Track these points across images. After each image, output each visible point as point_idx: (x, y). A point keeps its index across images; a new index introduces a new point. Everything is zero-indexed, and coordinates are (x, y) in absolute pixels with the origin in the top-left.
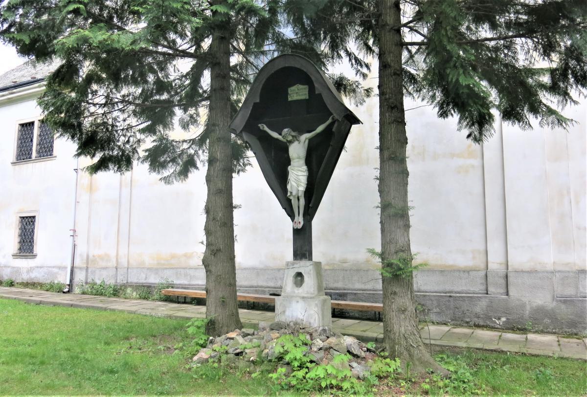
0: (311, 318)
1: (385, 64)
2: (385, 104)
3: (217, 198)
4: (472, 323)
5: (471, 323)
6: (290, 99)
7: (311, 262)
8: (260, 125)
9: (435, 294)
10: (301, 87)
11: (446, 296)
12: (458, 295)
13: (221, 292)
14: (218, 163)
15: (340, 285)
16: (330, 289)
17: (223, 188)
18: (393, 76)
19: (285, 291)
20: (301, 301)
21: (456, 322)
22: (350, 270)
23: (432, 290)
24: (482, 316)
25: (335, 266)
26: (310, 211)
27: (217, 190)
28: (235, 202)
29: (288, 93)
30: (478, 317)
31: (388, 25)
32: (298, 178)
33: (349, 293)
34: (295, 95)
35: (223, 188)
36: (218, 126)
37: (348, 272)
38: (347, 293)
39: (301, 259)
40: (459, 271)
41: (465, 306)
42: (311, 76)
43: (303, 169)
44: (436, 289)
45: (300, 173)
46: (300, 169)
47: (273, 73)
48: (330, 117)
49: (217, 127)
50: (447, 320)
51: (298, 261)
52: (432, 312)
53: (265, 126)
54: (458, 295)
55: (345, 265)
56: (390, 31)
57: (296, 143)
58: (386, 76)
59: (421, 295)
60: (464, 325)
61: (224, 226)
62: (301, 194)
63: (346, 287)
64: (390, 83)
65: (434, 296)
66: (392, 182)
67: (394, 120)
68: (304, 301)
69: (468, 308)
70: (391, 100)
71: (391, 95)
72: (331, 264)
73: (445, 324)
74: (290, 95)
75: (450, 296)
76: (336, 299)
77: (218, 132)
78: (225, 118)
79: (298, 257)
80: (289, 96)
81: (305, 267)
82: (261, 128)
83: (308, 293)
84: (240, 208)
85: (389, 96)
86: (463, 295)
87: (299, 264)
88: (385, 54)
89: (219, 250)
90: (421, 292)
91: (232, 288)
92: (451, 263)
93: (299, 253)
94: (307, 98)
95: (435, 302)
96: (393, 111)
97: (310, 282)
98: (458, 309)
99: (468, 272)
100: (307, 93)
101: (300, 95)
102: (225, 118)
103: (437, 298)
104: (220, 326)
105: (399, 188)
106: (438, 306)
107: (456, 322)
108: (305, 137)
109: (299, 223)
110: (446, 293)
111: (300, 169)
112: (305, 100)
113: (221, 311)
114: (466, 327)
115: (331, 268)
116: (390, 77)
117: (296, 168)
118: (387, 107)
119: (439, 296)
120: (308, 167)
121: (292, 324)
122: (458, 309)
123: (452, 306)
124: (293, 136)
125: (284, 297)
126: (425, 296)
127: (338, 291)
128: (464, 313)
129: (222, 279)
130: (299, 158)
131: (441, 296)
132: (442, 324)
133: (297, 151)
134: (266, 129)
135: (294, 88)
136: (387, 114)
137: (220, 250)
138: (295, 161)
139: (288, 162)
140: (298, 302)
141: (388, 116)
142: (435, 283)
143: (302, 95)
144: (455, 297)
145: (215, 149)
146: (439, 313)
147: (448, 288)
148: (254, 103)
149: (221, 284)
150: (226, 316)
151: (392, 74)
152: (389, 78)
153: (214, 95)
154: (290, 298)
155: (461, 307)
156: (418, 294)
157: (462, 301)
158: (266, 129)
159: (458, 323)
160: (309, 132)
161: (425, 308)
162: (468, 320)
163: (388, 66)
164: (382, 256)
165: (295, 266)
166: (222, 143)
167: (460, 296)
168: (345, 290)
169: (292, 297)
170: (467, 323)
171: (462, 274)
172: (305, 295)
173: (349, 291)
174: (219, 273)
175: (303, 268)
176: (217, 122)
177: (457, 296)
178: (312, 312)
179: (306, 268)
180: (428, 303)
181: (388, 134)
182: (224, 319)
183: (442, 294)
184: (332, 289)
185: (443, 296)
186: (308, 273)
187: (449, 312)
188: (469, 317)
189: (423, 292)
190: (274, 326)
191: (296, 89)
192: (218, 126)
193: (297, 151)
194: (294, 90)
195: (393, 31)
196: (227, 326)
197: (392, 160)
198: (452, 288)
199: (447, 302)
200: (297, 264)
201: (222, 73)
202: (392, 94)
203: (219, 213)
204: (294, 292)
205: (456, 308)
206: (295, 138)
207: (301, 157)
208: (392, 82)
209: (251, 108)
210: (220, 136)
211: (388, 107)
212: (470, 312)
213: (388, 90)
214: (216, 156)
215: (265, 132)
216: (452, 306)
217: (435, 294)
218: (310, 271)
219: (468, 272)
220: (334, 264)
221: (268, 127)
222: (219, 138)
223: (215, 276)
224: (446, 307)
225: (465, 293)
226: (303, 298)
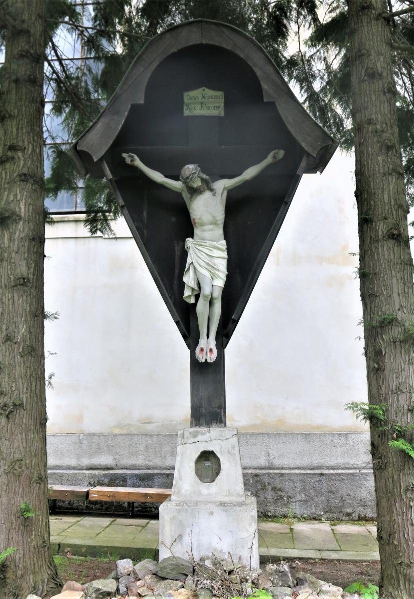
0: (243, 547)
1: (371, 71)
2: (375, 139)
3: (16, 295)
4: (355, 516)
5: (353, 515)
6: (186, 113)
7: (226, 433)
8: (124, 155)
9: (296, 471)
10: (209, 92)
11: (314, 474)
12: (332, 471)
13: (22, 497)
14: (21, 222)
15: (140, 461)
16: (122, 469)
17: (31, 276)
18: (387, 94)
19: (179, 492)
20: (217, 510)
21: (331, 515)
22: (157, 435)
23: (292, 465)
24: (369, 503)
25: (132, 429)
26: (225, 333)
27: (19, 279)
28: (48, 308)
29: (183, 102)
30: (365, 506)
31: (374, 9)
32: (207, 261)
33: (157, 474)
34: (199, 107)
35: (31, 276)
36: (23, 150)
37: (155, 438)
38: (153, 475)
39: (209, 423)
40: (333, 434)
41: (344, 489)
42: (254, 68)
43: (222, 245)
44: (298, 462)
45: (216, 253)
46: (215, 244)
47: (175, 52)
48: (274, 150)
49: (20, 154)
50: (319, 512)
51: (204, 429)
52: (294, 500)
53: (136, 157)
54: (332, 471)
55: (150, 427)
56: (377, 19)
57: (207, 195)
58: (374, 92)
59: (276, 474)
60: (344, 518)
61: (30, 354)
62: (218, 294)
63: (150, 464)
64: (382, 106)
65: (297, 474)
66: (394, 280)
67: (394, 170)
68: (226, 511)
69: (348, 492)
70: (385, 135)
71: (384, 126)
72: (126, 426)
73: (315, 519)
74: (188, 105)
75: (322, 474)
76: (134, 486)
77: (22, 163)
78: (35, 138)
79: (203, 421)
80: (185, 108)
81: (210, 438)
82: (128, 161)
83: (230, 494)
84: (56, 318)
85: (382, 127)
86: (340, 471)
87: (208, 434)
88: (369, 55)
89: (18, 406)
90: (274, 469)
91: (42, 486)
92: (319, 421)
93: (204, 411)
94: (222, 114)
95: (298, 485)
96: (390, 153)
97: (231, 475)
98: (334, 493)
99: (346, 435)
100: (222, 105)
101: (207, 108)
102: (35, 138)
103: (301, 477)
104: (19, 573)
105: (406, 290)
106: (304, 490)
107: (331, 515)
108: (222, 185)
109: (211, 350)
110: (312, 469)
111: (215, 244)
112: (219, 117)
113: (20, 538)
114: (347, 522)
115: (124, 432)
116: (382, 96)
117: (208, 243)
118: (379, 145)
119: (304, 474)
120: (228, 243)
121: (208, 563)
122: (334, 493)
123: (324, 490)
124: (203, 180)
125: (178, 505)
126: (282, 475)
127: (136, 472)
128: (344, 499)
129: (24, 468)
130: (215, 223)
131: (307, 474)
132: (311, 519)
133: (208, 209)
134: (138, 163)
135: (197, 93)
136: (380, 158)
137: (21, 405)
138: (206, 227)
139: (187, 228)
140: (212, 513)
141: (381, 162)
142: (296, 453)
143: (213, 108)
144: (329, 475)
145: (16, 195)
146: (304, 502)
147: (316, 461)
148: (133, 106)
149: (22, 478)
150: (32, 549)
151: (386, 90)
152: (379, 96)
153: (14, 92)
154: (191, 506)
155: (338, 491)
156: (271, 471)
157: (339, 480)
158: (138, 163)
159: (335, 515)
160: (230, 177)
161: (282, 494)
162: (349, 510)
163: (377, 75)
164: (372, 418)
165: (200, 438)
166: (29, 186)
167: (336, 474)
168: (149, 469)
169: (196, 503)
170: (349, 515)
171: (337, 439)
172: (226, 499)
173: (156, 471)
174: (17, 456)
175: (217, 442)
176: (20, 143)
177: (332, 474)
178: (244, 535)
179: (223, 443)
180: (288, 486)
181: (383, 192)
182: (27, 556)
183: (309, 472)
184: (126, 469)
185: (310, 474)
186: (229, 453)
187: (320, 500)
188: (350, 505)
189: (278, 469)
190: (168, 570)
191: (201, 97)
192: (23, 150)
193: (208, 209)
194: (196, 98)
195: (382, 19)
196: (34, 573)
197: (393, 238)
198: (322, 461)
199: (317, 484)
200: (203, 434)
201: (32, 51)
202: (387, 124)
203: (20, 327)
204: (200, 493)
205: (331, 492)
206: (207, 186)
207: (219, 222)
208: (386, 104)
209: (126, 113)
210: (25, 171)
211: (382, 145)
212: (351, 497)
213: (379, 116)
214: (17, 210)
215: (136, 169)
216: (324, 490)
217: (296, 471)
218: (233, 447)
219: (346, 435)
220: (130, 425)
221: (141, 160)
222: (25, 175)
223: (8, 463)
224: (316, 491)
225: (343, 469)
226: (222, 504)
